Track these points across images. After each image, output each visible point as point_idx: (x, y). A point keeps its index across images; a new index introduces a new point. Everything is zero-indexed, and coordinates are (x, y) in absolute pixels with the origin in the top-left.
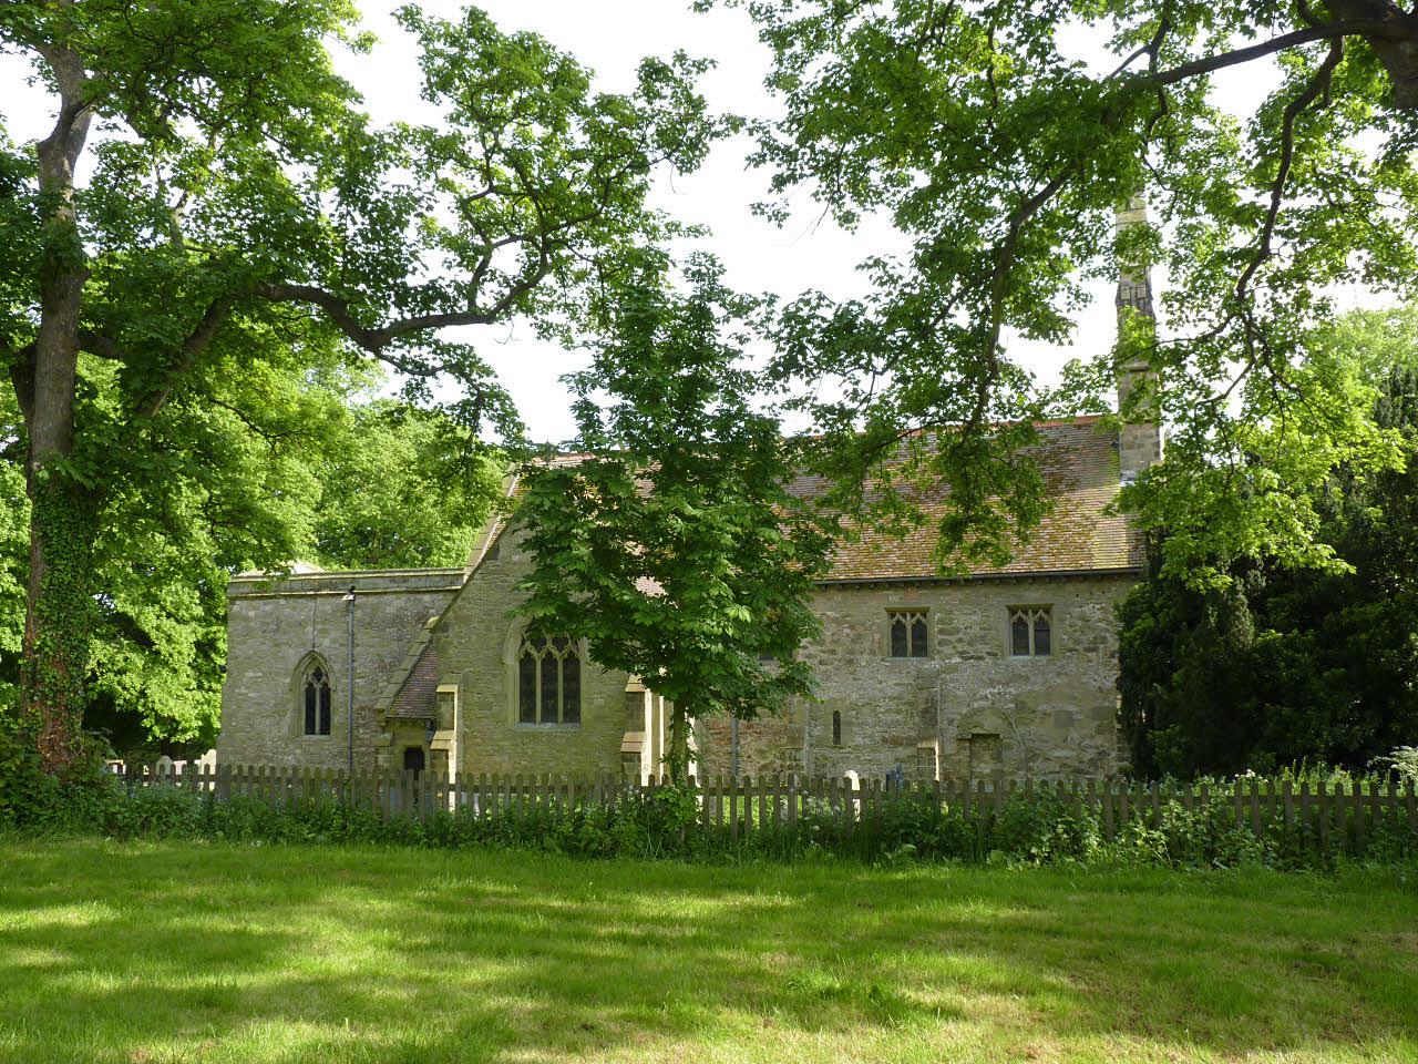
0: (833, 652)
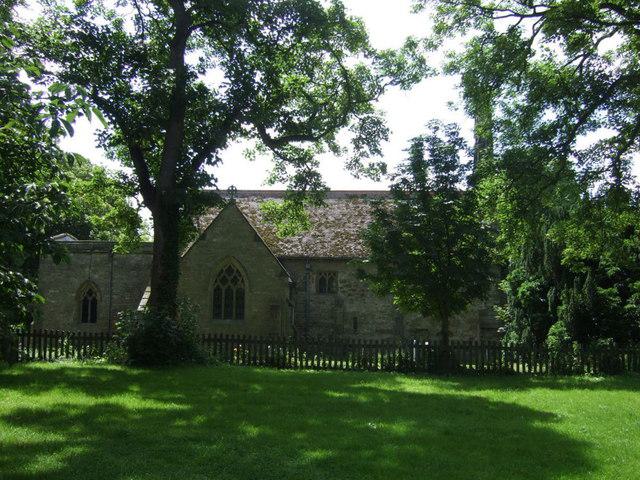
0: (354, 290)
